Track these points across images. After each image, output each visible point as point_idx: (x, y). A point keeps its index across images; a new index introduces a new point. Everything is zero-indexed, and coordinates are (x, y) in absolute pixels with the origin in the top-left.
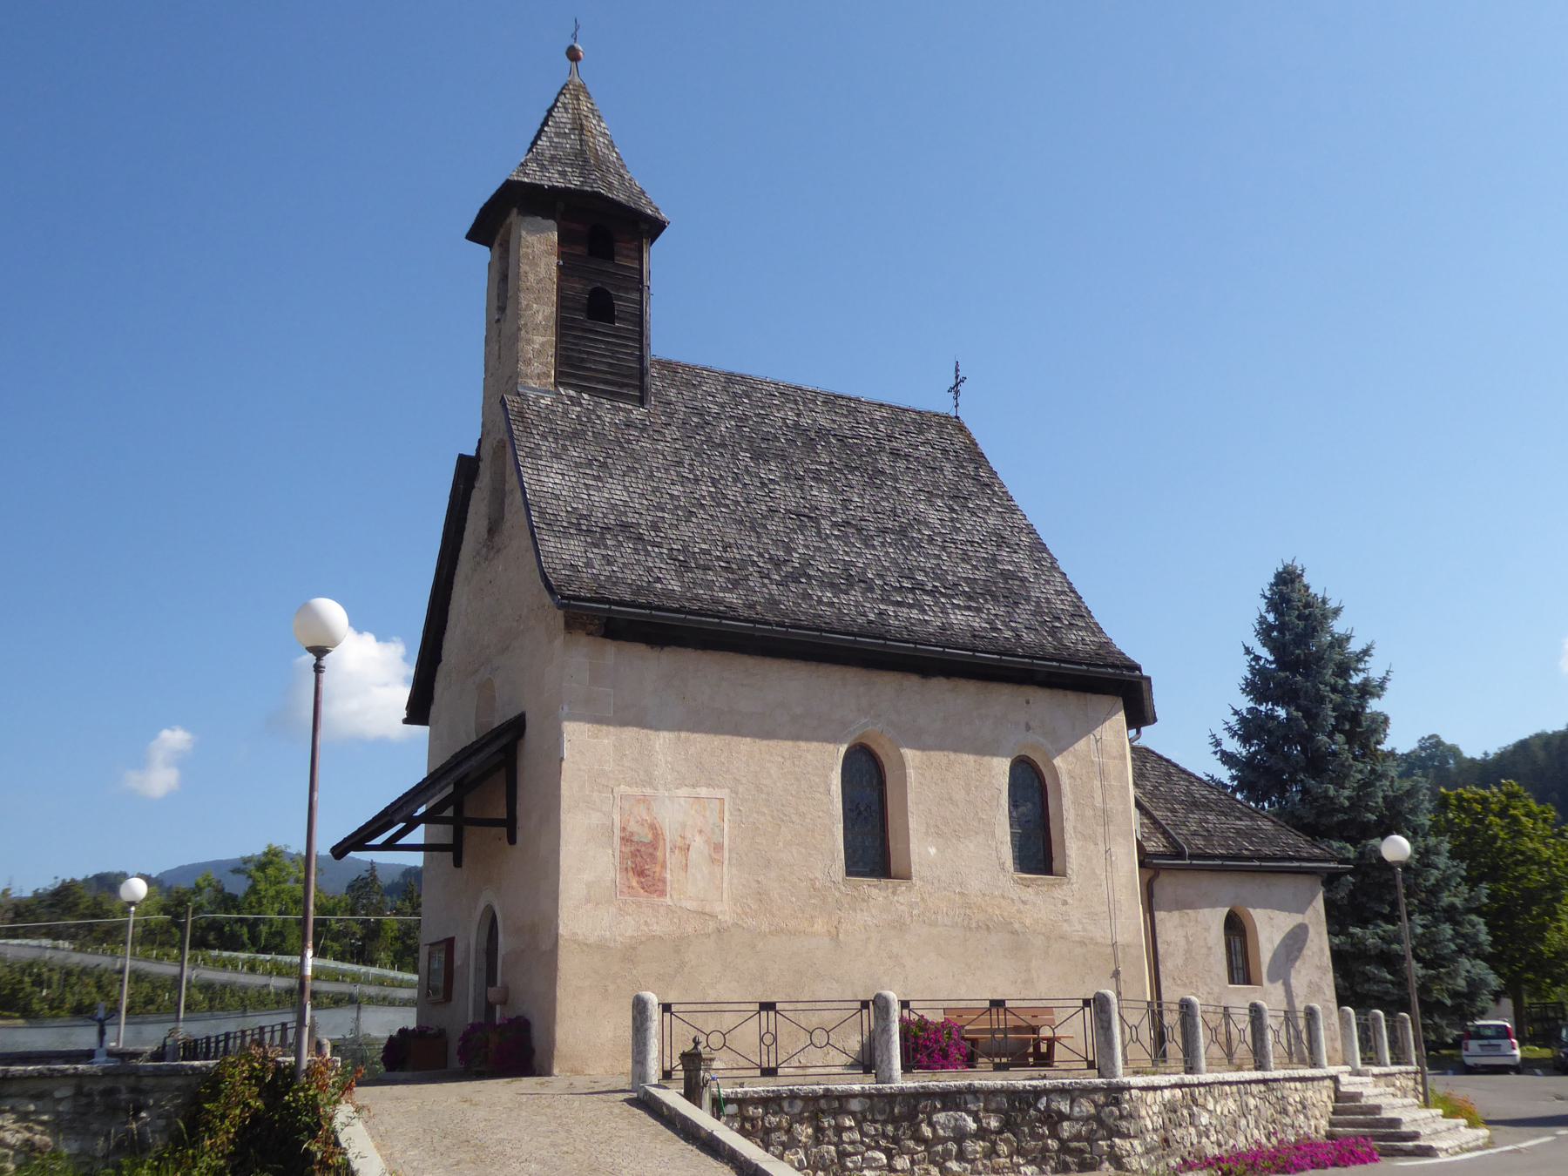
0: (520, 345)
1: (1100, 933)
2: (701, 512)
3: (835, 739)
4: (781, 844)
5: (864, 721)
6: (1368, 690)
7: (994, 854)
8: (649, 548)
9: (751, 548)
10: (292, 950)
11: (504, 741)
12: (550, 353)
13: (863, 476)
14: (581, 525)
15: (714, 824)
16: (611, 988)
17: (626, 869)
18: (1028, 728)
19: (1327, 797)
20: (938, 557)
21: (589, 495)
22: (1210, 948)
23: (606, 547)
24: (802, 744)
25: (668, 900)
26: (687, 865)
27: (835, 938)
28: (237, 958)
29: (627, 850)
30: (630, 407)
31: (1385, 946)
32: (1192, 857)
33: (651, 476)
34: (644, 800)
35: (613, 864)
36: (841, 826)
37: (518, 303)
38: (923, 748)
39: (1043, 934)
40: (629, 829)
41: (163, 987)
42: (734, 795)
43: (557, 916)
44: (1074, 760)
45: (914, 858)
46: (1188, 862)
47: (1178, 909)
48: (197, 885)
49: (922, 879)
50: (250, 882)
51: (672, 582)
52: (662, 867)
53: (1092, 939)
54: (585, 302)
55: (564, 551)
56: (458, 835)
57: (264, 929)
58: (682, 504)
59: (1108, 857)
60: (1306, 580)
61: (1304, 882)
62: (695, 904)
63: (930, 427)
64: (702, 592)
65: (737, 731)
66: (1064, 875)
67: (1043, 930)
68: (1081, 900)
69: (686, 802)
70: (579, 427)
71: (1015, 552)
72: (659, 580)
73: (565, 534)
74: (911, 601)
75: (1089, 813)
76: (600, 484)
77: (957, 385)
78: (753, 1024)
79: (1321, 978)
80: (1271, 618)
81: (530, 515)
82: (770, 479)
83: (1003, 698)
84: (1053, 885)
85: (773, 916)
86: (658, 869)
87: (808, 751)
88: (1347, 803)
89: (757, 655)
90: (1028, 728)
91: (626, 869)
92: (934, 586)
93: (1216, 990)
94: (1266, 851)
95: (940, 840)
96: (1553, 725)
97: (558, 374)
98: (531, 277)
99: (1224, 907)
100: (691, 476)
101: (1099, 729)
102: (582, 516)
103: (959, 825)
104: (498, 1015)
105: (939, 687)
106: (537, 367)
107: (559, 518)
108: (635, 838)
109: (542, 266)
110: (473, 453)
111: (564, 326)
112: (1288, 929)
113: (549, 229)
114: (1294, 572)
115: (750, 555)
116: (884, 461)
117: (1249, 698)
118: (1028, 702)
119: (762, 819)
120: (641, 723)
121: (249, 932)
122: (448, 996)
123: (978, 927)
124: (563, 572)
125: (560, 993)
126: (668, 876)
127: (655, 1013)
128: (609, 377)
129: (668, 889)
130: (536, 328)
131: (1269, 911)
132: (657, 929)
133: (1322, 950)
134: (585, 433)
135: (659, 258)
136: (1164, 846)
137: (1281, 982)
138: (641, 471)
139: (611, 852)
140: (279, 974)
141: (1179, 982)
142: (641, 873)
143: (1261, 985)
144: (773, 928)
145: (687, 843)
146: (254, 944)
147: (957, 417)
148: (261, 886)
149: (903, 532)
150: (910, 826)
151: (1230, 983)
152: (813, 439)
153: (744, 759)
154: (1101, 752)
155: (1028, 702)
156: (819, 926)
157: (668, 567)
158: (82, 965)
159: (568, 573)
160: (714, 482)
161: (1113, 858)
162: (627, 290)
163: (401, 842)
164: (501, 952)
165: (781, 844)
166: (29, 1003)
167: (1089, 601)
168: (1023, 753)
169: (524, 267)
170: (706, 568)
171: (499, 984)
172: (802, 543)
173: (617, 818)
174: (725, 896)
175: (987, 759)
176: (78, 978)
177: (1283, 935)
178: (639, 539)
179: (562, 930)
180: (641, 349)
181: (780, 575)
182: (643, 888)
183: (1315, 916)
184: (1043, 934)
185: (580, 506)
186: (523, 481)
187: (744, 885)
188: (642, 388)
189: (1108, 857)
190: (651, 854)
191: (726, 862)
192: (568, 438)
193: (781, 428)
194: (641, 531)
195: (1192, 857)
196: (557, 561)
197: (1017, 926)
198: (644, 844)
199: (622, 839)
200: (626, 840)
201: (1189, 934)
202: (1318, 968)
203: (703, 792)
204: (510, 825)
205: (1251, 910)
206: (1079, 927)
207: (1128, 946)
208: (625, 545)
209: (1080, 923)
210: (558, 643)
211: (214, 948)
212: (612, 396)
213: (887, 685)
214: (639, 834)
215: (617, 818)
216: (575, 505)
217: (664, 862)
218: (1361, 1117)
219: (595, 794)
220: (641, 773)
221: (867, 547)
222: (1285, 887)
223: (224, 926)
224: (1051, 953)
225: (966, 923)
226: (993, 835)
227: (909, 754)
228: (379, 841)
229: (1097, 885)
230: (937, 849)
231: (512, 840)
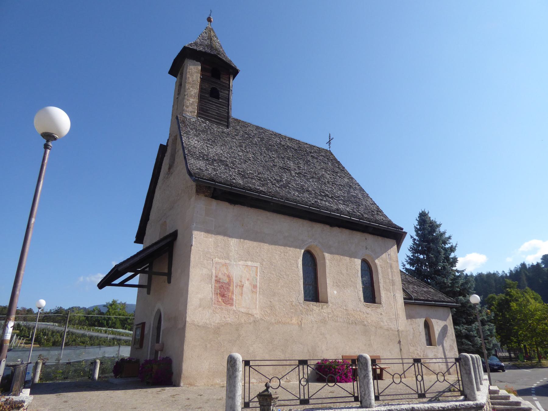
0: (185, 100)
1: (393, 326)
2: (249, 161)
3: (300, 248)
4: (279, 287)
5: (310, 240)
6: (452, 249)
7: (357, 294)
8: (231, 169)
9: (268, 175)
10: (118, 327)
11: (168, 240)
12: (196, 105)
13: (304, 161)
14: (204, 157)
15: (253, 277)
16: (209, 346)
17: (217, 293)
18: (367, 249)
19: (444, 283)
20: (332, 188)
21: (207, 149)
22: (420, 333)
23: (214, 166)
24: (288, 248)
25: (234, 308)
27: (300, 325)
28: (102, 329)
29: (218, 285)
30: (224, 128)
31: (468, 332)
32: (415, 300)
33: (231, 148)
34: (225, 265)
36: (302, 281)
37: (185, 87)
38: (331, 253)
39: (374, 326)
40: (219, 277)
41: (79, 337)
42: (261, 265)
43: (186, 313)
44: (382, 261)
45: (329, 295)
46: (413, 301)
47: (410, 319)
48: (94, 310)
49: (332, 303)
50: (108, 309)
51: (240, 181)
52: (232, 294)
53: (391, 328)
54: (209, 91)
55: (197, 165)
56: (150, 280)
57: (110, 322)
58: (242, 158)
59: (395, 298)
60: (429, 215)
61: (447, 310)
62: (245, 310)
63: (322, 152)
64: (251, 185)
65: (262, 240)
66: (380, 303)
67: (374, 325)
68: (387, 313)
69: (242, 267)
70: (205, 129)
71: (355, 190)
72: (234, 179)
73: (198, 159)
74: (325, 200)
75: (388, 281)
76: (212, 147)
77: (330, 141)
78: (295, 374)
79: (453, 344)
80: (418, 227)
81: (184, 151)
82: (272, 157)
83: (358, 237)
84: (377, 307)
85: (277, 316)
86: (230, 294)
87: (290, 250)
88: (450, 285)
89: (271, 212)
90: (367, 249)
91: (217, 293)
92: (332, 196)
93: (423, 348)
94: (435, 298)
95: (338, 288)
96: (547, 253)
97: (198, 113)
98: (191, 79)
99: (424, 318)
100: (245, 151)
101: (389, 250)
102: (206, 155)
103: (344, 283)
104: (159, 356)
105: (336, 230)
106: (190, 109)
107: (196, 154)
108: (221, 281)
109: (195, 76)
110: (165, 144)
111: (201, 98)
112: (442, 326)
113: (198, 65)
114: (425, 213)
115: (268, 177)
116: (309, 158)
117: (411, 252)
118: (366, 239)
119: (272, 276)
120: (225, 234)
121: (106, 322)
122: (141, 346)
123: (352, 323)
124: (196, 170)
125: (185, 347)
126: (234, 298)
127: (240, 366)
128: (216, 117)
129: (234, 303)
130: (191, 96)
131: (437, 320)
132: (229, 320)
133: (452, 334)
134: (207, 131)
135: (235, 83)
136: (405, 295)
137: (441, 345)
138: (227, 146)
139: (211, 286)
140: (113, 334)
141: (412, 345)
142: (223, 296)
143: (436, 346)
144: (276, 321)
145: (243, 284)
146: (107, 326)
147: (330, 151)
148: (111, 310)
149: (319, 179)
150: (327, 282)
151: (427, 346)
152: (286, 148)
153: (266, 252)
154: (390, 259)
155: (366, 239)
156: (294, 321)
157: (238, 176)
158: (58, 330)
159: (198, 171)
160: (254, 154)
161: (396, 298)
162: (224, 90)
163: (127, 283)
164: (162, 328)
165: (279, 287)
166: (41, 340)
167: (381, 208)
168: (364, 258)
169: (188, 76)
170: (252, 179)
171: (160, 342)
172: (285, 177)
173: (214, 272)
174: (257, 307)
175: (353, 259)
176: (56, 333)
177: (441, 328)
178: (227, 165)
179: (188, 319)
180: (228, 110)
181: (279, 185)
182: (224, 302)
183: (449, 322)
184: (374, 326)
185: (204, 152)
186: (182, 140)
187: (265, 303)
188: (228, 122)
189: (395, 298)
190: (228, 288)
191: (258, 293)
192: (201, 131)
193: (275, 144)
194: (227, 163)
195: (415, 300)
196: (194, 167)
197: (365, 323)
198: (225, 283)
199: (216, 280)
200: (217, 281)
201: (414, 327)
202: (452, 340)
203: (249, 263)
204: (169, 275)
205: (431, 319)
206: (386, 324)
207: (403, 331)
208: (221, 166)
209: (387, 322)
210: (193, 199)
211: (96, 326)
212: (217, 123)
213: (318, 229)
214: (223, 279)
215: (214, 272)
216: (202, 151)
217: (233, 291)
218: (504, 401)
219: (205, 261)
220: (225, 254)
221: (308, 181)
222: (441, 311)
223: (100, 321)
224: (377, 334)
225: (348, 321)
226: (356, 287)
227: (327, 255)
228: (117, 281)
229: (391, 308)
230: (337, 292)
231: (169, 282)
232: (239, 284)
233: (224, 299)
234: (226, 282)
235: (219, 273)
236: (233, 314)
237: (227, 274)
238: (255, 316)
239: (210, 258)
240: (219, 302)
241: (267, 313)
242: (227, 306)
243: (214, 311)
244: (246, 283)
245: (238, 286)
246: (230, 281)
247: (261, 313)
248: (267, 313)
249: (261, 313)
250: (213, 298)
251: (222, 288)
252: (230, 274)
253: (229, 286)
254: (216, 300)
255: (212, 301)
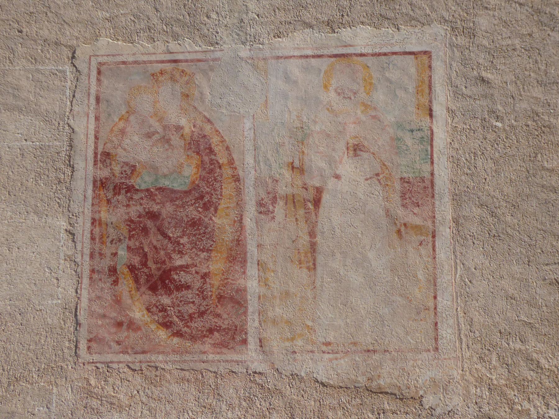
15: (400, 126)
17: (113, 271)
26: (313, 246)
35: (70, 259)
40: (122, 155)
42: (461, 40)
62: (344, 363)
69: (306, 70)
91: (113, 271)
139: (63, 224)
182: (167, 325)
190: (194, 224)
217: (239, 242)
232: (282, 190)
233: (166, 300)
234: (176, 186)
235: (123, 132)
236: (250, 400)
237: (187, 131)
238: (429, 400)
239: (57, 44)
240: (132, 325)
241: (530, 375)
242: (198, 346)
243: (90, 394)
244: (338, 177)
245: (281, 203)
246: (211, 171)
247: (480, 380)
248: (530, 375)
249: (480, 380)
250: (84, 303)
251: (153, 230)
252: (208, 128)
253: (206, 207)
254: (104, 316)
255: (78, 324)
